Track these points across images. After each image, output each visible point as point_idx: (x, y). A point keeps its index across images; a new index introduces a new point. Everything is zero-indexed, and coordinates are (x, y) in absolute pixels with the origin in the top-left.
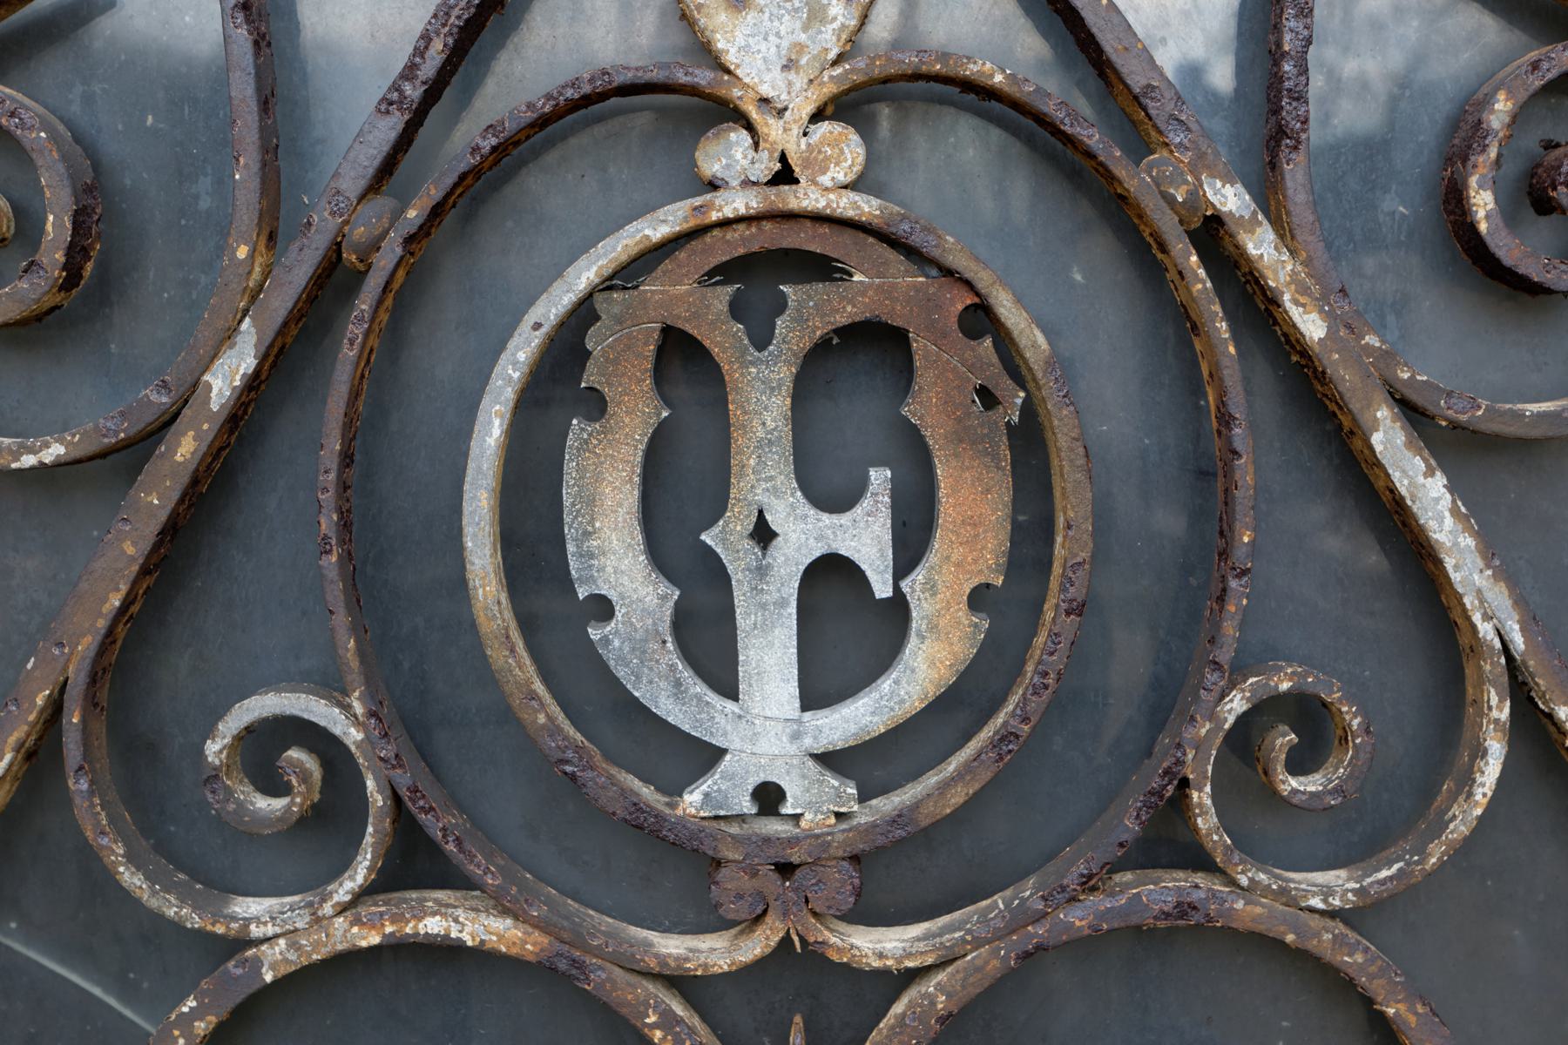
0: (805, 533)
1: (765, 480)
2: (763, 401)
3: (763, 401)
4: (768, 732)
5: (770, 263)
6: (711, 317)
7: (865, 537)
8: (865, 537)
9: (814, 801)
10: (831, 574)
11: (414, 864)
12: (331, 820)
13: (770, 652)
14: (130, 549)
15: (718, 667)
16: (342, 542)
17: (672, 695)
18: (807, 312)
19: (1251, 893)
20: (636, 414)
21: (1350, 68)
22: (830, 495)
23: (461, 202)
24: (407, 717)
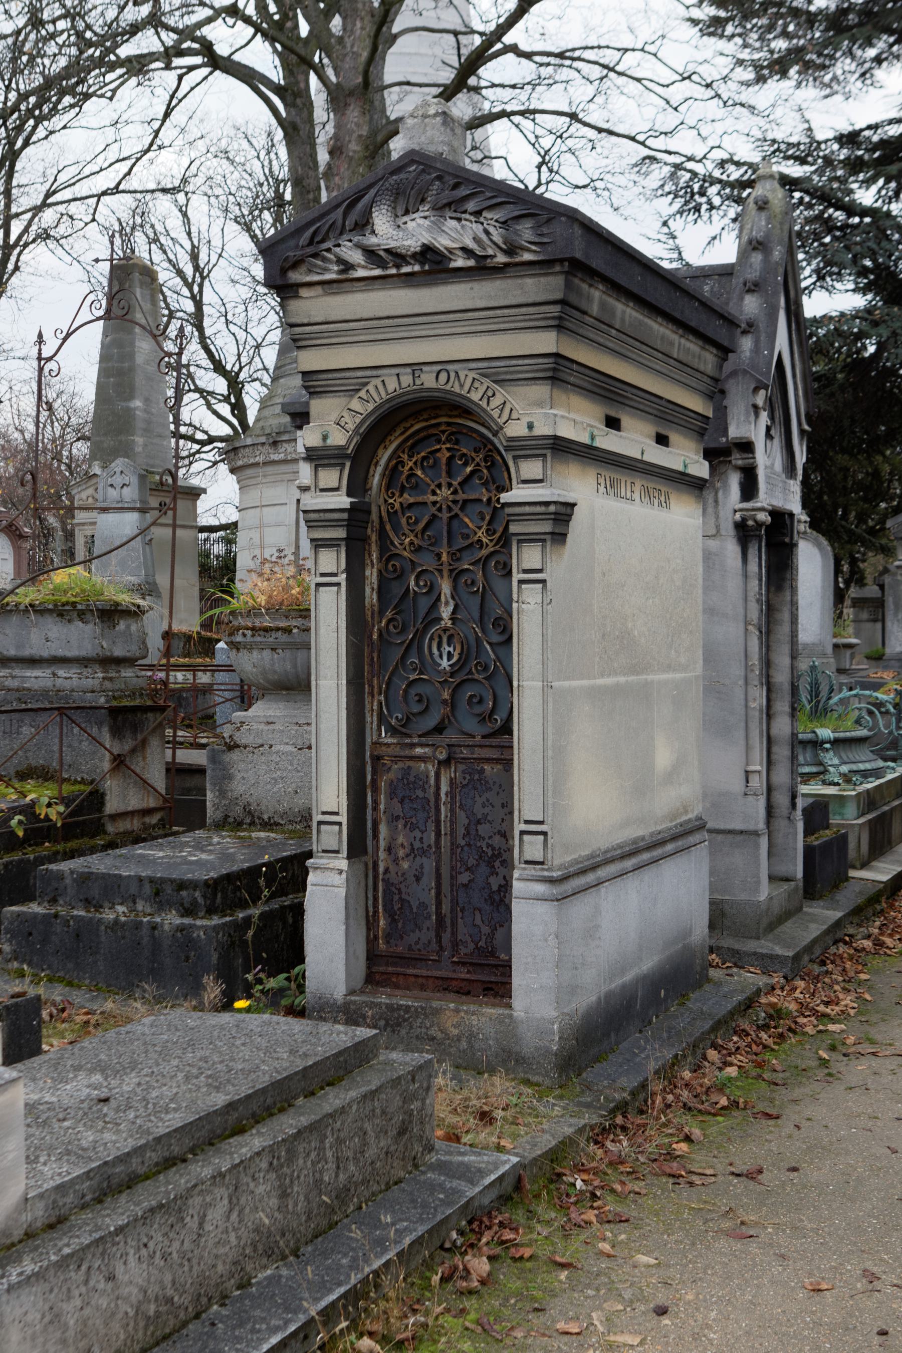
0: (447, 649)
1: (445, 645)
2: (445, 640)
3: (445, 640)
4: (445, 663)
5: (445, 630)
6: (442, 633)
7: (451, 649)
8: (451, 649)
9: (448, 668)
10: (449, 652)
11: (421, 673)
12: (415, 670)
13: (445, 657)
14: (896, 309)
15: (441, 656)
16: (453, 598)
17: (438, 660)
18: (448, 633)
19: (476, 676)
20: (437, 640)
21: (89, 647)
22: (449, 646)
23: (739, 693)
24: (422, 662)
